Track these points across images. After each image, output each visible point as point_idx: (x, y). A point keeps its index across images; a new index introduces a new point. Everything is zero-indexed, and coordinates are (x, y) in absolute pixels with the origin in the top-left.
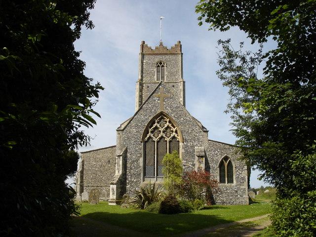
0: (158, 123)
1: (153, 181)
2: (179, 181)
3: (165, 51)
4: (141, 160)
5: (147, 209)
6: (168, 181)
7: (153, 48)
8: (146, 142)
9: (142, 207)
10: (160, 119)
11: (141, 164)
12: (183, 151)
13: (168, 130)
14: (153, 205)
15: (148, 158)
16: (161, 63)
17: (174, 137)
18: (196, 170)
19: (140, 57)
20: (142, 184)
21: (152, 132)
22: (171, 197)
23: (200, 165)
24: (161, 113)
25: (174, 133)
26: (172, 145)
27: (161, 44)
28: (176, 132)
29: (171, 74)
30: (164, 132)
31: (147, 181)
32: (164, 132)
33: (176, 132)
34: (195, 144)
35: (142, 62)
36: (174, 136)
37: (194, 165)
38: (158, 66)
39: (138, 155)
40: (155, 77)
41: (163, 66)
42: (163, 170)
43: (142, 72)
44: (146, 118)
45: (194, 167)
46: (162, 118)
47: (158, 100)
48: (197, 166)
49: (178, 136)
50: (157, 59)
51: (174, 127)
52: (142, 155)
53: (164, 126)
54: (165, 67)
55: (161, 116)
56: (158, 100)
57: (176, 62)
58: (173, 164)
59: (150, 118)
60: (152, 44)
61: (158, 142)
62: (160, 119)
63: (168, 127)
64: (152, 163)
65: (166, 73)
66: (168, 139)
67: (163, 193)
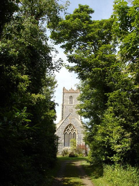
0: (69, 127)
1: (67, 148)
2: (75, 148)
3: (73, 92)
4: (63, 140)
5: (65, 156)
6: (72, 148)
7: (68, 90)
8: (65, 134)
9: (64, 156)
10: (70, 126)
11: (63, 142)
13: (73, 130)
14: (67, 155)
16: (71, 97)
17: (74, 133)
18: (82, 144)
19: (62, 94)
20: (63, 149)
21: (67, 131)
22: (72, 153)
24: (70, 124)
27: (72, 88)
28: (75, 131)
30: (71, 131)
31: (65, 148)
32: (71, 131)
33: (75, 131)
35: (63, 96)
37: (81, 142)
38: (70, 98)
40: (69, 103)
41: (72, 98)
42: (70, 144)
43: (63, 100)
46: (70, 126)
48: (82, 143)
50: (70, 95)
58: (73, 142)
59: (66, 126)
60: (68, 88)
61: (69, 134)
62: (70, 126)
63: (72, 129)
65: (73, 101)
66: (72, 133)
67: (70, 152)
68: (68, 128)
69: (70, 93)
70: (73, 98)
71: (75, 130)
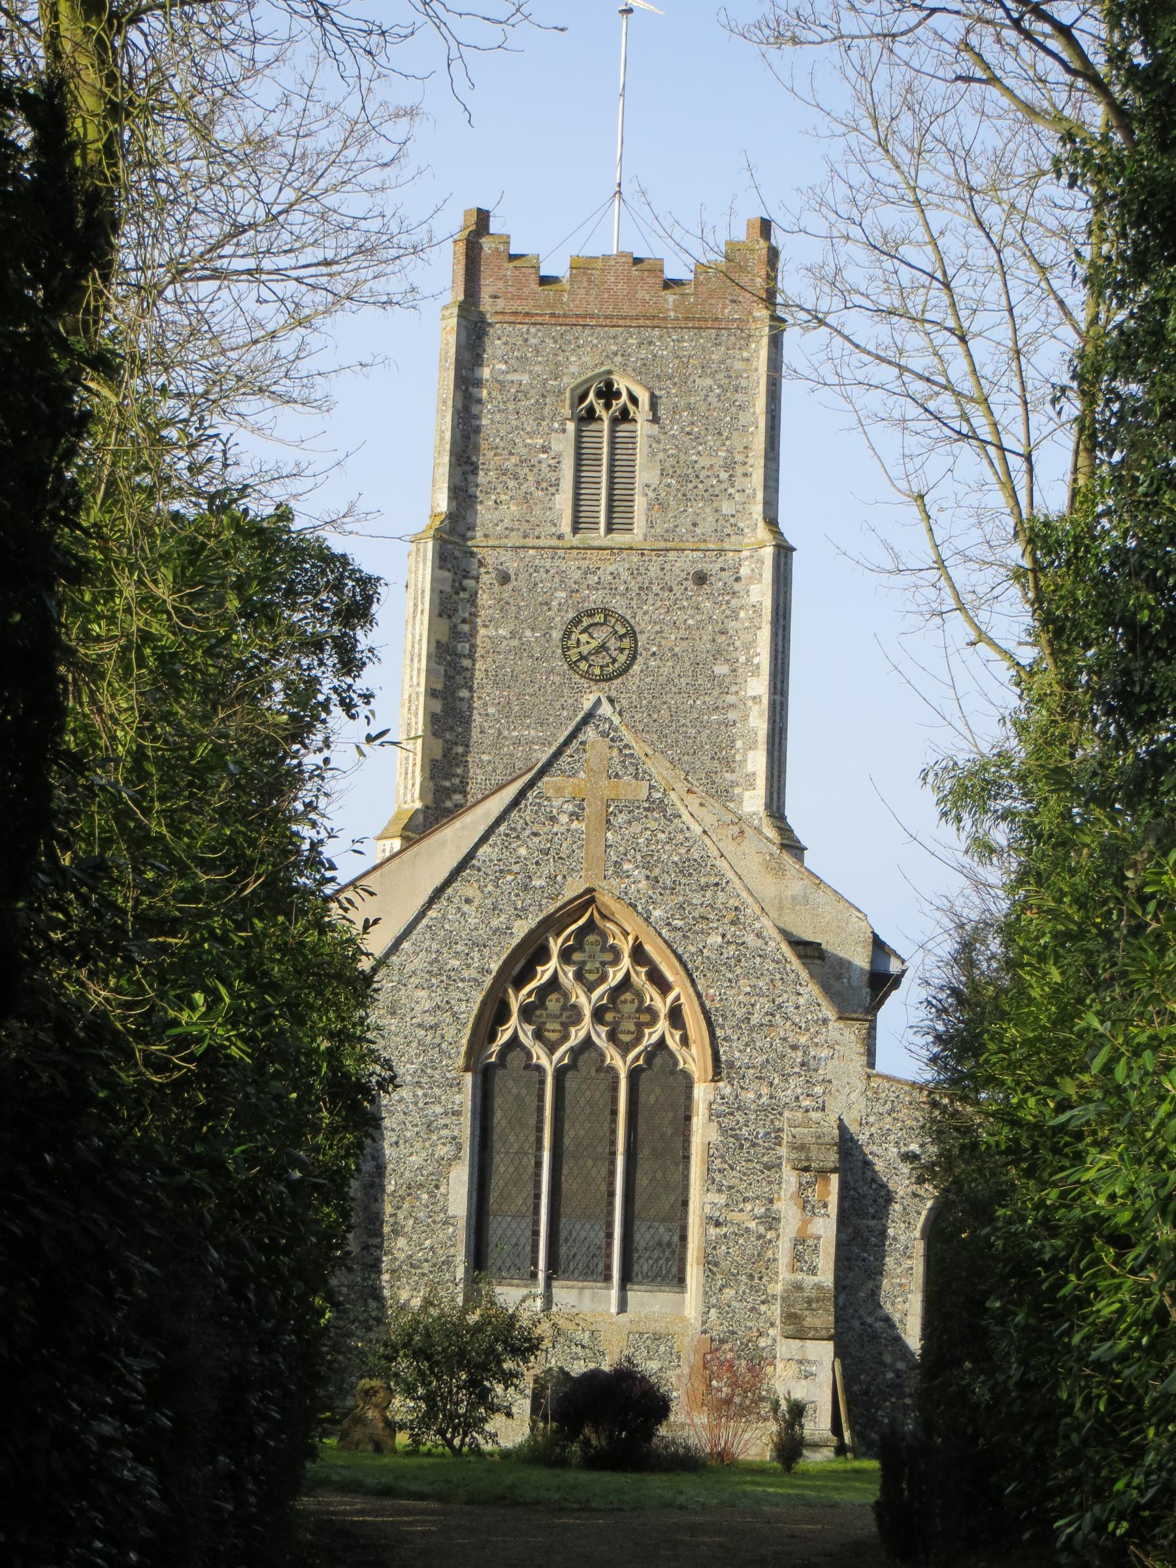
12: (714, 1136)
15: (502, 1166)
16: (608, 393)
21: (527, 1013)
23: (805, 1223)
25: (662, 1025)
26: (649, 1098)
29: (684, 481)
33: (675, 1016)
34: (785, 1096)
36: (662, 1042)
37: (771, 1221)
38: (590, 416)
39: (443, 1151)
40: (563, 501)
41: (624, 416)
44: (495, 923)
45: (770, 1235)
47: (575, 816)
49: (685, 1041)
51: (664, 986)
52: (466, 1153)
53: (603, 978)
54: (642, 426)
55: (579, 923)
56: (575, 816)
57: (732, 385)
59: (521, 929)
64: (520, 1201)
65: (645, 474)
68: (553, 963)
69: (581, 320)
70: (642, 413)
71: (662, 1006)
